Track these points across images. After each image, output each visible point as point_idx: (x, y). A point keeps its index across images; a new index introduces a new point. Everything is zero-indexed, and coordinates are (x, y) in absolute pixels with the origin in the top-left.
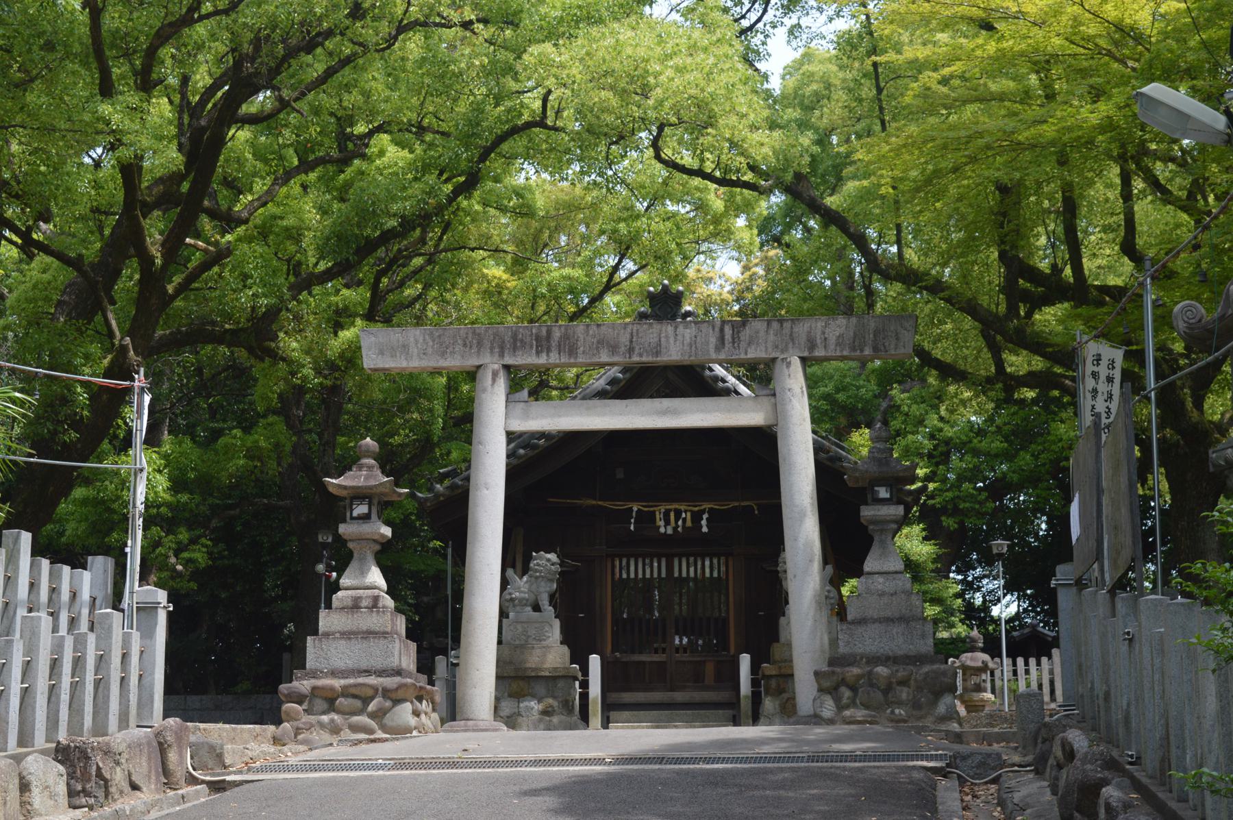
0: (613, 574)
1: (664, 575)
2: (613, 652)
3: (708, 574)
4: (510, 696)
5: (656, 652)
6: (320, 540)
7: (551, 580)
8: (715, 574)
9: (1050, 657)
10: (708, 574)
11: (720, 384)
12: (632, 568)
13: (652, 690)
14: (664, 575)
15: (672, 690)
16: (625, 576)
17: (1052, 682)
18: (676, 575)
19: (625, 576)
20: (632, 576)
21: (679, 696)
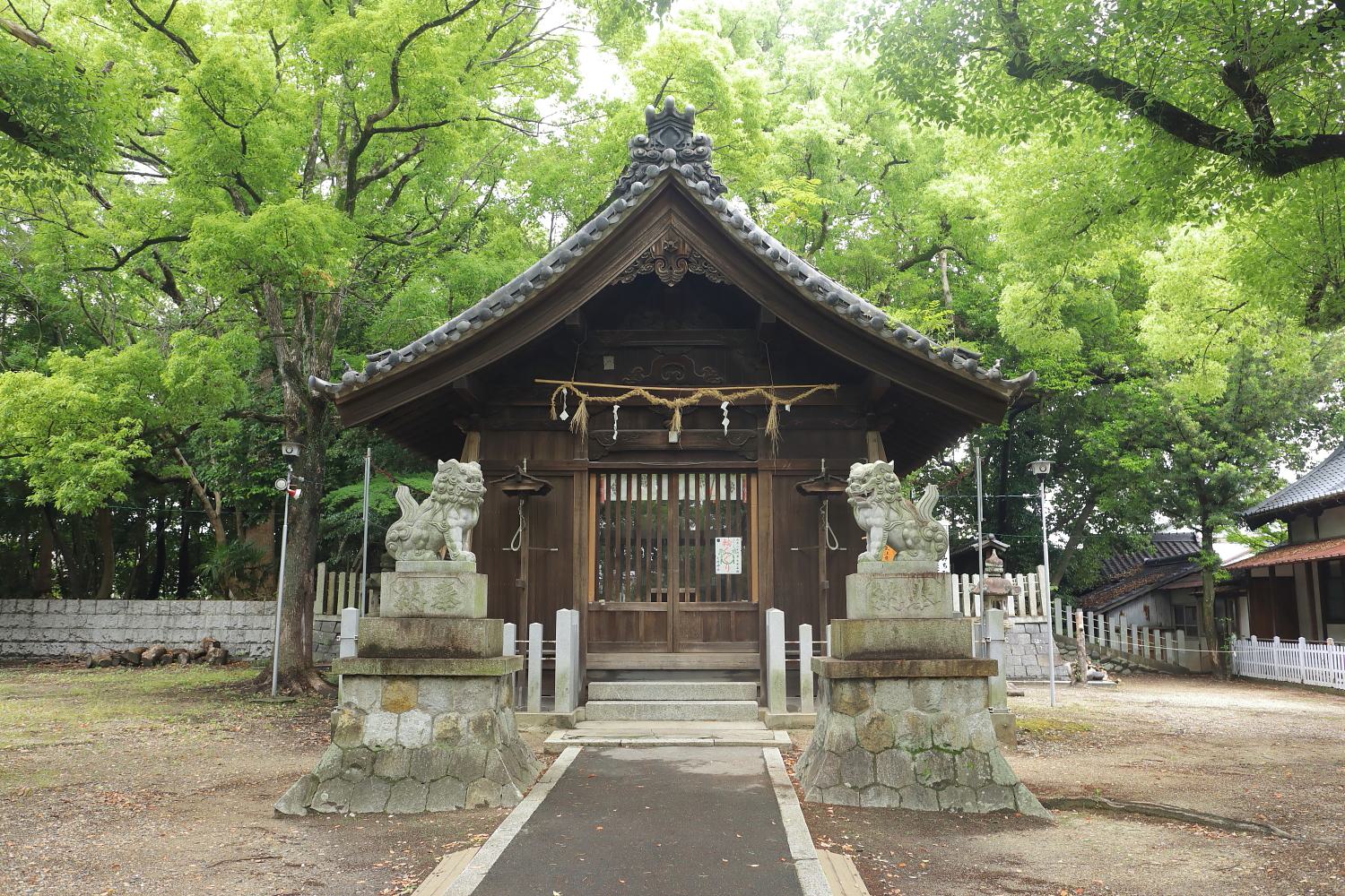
0: (599, 494)
1: (665, 497)
2: (597, 597)
3: (723, 497)
4: (384, 708)
5: (654, 599)
6: (284, 452)
7: (470, 507)
8: (733, 497)
9: (1035, 571)
10: (723, 497)
11: (743, 235)
12: (655, 488)
13: (648, 649)
14: (665, 497)
15: (674, 650)
16: (613, 498)
17: (1038, 596)
18: (682, 496)
19: (613, 498)
20: (624, 497)
21: (686, 660)
